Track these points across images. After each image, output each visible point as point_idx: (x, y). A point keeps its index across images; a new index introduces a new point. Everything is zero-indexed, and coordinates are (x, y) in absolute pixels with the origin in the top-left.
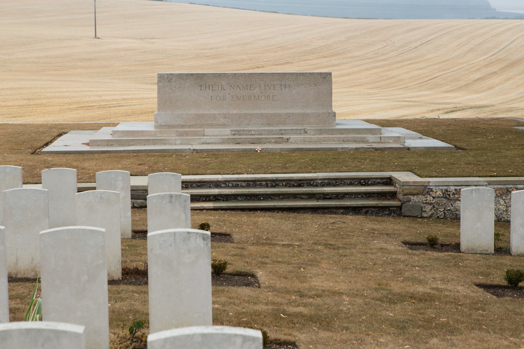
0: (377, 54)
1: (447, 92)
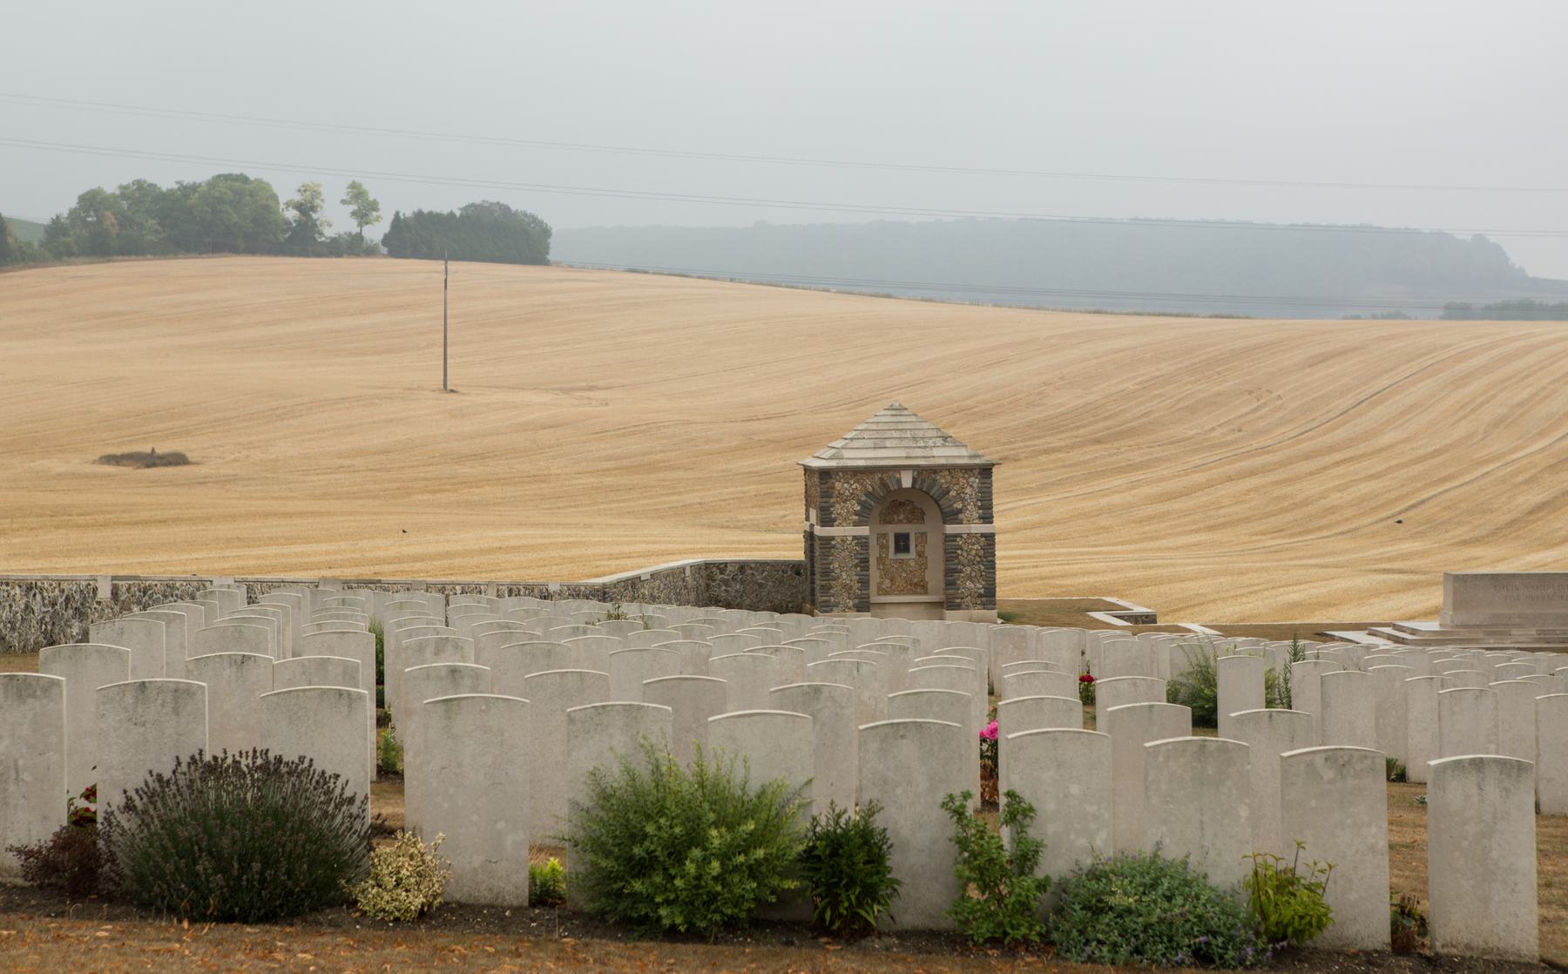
0: (1240, 431)
1: (1465, 543)
